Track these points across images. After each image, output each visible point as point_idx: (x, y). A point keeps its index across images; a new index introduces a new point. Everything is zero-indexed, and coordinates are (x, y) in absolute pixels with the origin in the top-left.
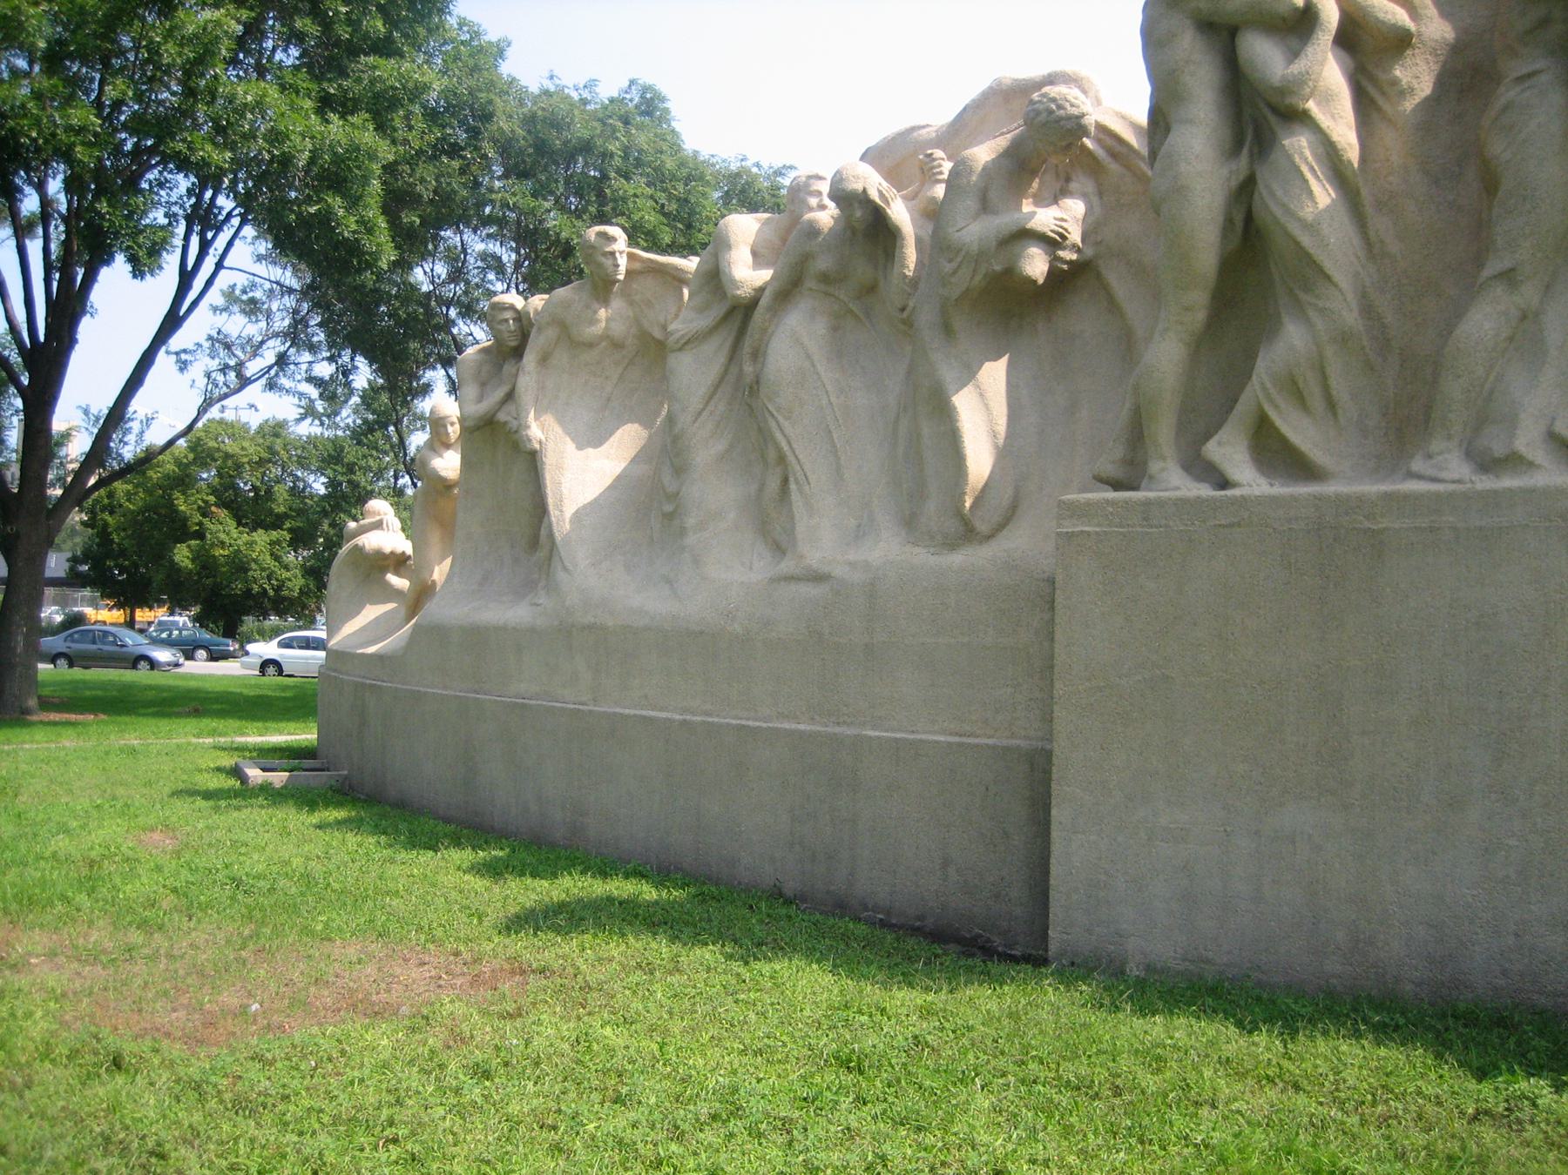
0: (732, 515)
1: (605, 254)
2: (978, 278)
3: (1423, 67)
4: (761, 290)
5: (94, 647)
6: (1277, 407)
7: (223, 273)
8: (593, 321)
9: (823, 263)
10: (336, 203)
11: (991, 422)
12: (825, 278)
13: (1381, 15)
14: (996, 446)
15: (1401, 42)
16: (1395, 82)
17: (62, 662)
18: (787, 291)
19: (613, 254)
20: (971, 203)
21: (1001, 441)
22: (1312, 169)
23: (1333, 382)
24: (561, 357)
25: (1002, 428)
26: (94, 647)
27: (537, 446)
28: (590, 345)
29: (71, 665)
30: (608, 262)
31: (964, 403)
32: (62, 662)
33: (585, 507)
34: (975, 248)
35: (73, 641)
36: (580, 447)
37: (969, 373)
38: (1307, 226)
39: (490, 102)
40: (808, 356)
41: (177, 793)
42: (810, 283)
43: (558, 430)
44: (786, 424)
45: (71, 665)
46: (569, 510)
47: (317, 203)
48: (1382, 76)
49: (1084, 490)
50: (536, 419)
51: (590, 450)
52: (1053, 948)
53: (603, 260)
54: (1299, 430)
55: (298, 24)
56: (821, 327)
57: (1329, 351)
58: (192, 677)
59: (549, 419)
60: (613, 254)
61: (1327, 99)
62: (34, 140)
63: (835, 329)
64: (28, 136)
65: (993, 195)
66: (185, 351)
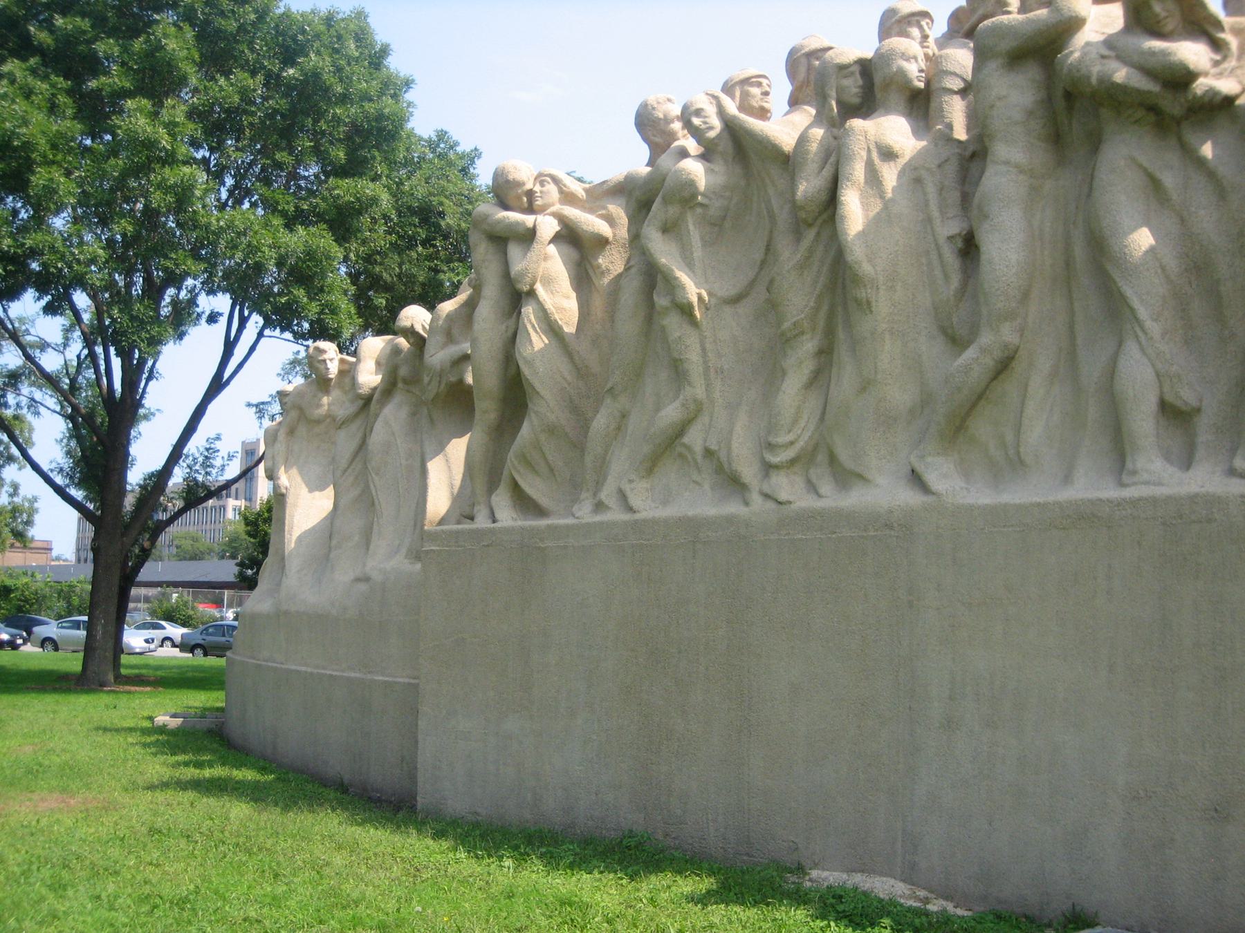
0: (356, 538)
1: (319, 361)
2: (443, 385)
3: (616, 255)
4: (375, 389)
5: (223, 639)
6: (518, 472)
7: (263, 340)
8: (319, 406)
9: (403, 371)
10: (300, 293)
11: (451, 478)
12: (405, 381)
13: (585, 227)
14: (452, 493)
15: (602, 242)
16: (599, 266)
17: (199, 651)
18: (389, 388)
19: (324, 361)
20: (440, 338)
21: (456, 491)
22: (533, 326)
23: (550, 458)
24: (302, 430)
25: (457, 483)
26: (223, 639)
27: (284, 491)
28: (318, 422)
29: (206, 655)
30: (322, 367)
31: (435, 468)
32: (199, 651)
33: (305, 532)
34: (438, 367)
35: (207, 634)
36: (311, 491)
37: (440, 448)
38: (527, 362)
39: (441, 204)
40: (393, 434)
41: (98, 729)
42: (400, 385)
43: (299, 479)
44: (376, 478)
45: (206, 655)
46: (296, 533)
47: (287, 295)
48: (595, 263)
49: (459, 523)
50: (286, 471)
51: (317, 493)
52: (419, 806)
53: (318, 365)
54: (534, 487)
55: (278, 156)
56: (404, 413)
57: (543, 437)
58: (163, 658)
59: (294, 472)
60: (324, 361)
61: (548, 281)
62: (61, 270)
63: (414, 414)
64: (56, 268)
65: (455, 332)
66: (263, 403)
